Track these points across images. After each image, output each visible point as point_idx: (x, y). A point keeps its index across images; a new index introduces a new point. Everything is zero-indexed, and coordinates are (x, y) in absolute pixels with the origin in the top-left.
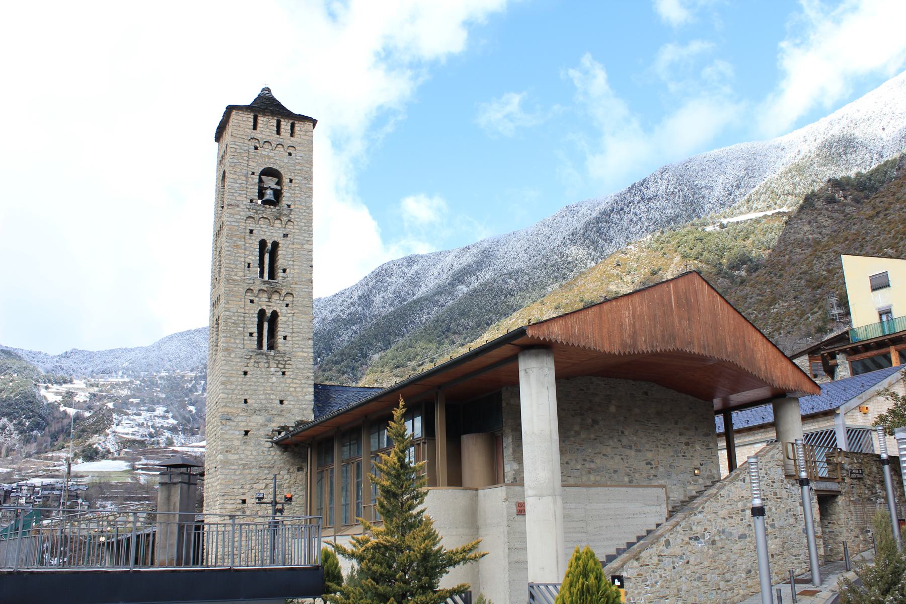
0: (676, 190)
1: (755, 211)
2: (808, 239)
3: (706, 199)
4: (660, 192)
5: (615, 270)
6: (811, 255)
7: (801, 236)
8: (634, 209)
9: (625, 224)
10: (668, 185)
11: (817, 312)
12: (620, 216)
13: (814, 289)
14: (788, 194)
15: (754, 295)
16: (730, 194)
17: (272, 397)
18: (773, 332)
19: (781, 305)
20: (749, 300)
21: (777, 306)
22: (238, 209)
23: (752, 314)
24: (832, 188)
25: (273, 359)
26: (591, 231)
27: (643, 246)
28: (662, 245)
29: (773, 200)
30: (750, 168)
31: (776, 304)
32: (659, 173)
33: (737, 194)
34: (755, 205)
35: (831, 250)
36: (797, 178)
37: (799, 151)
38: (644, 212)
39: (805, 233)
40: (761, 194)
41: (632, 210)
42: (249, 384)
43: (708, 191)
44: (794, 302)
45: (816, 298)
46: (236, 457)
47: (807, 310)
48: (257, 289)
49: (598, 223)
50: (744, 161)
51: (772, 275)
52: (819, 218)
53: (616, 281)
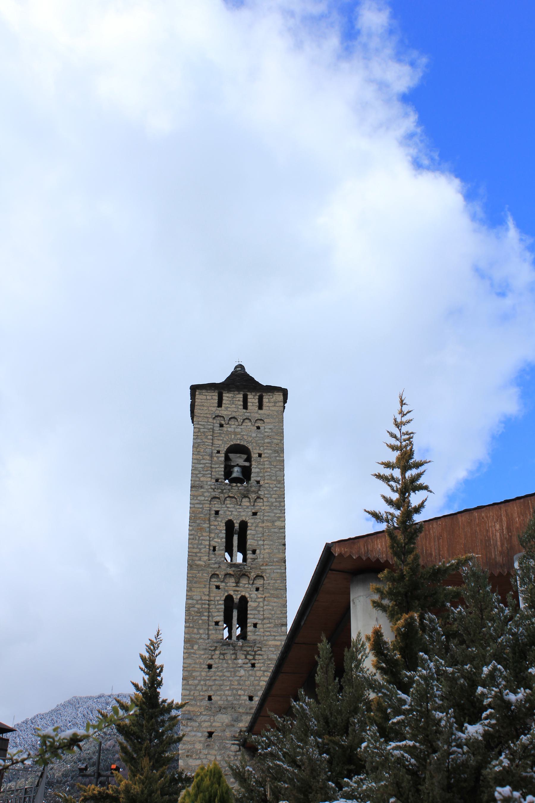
22: (202, 490)
48: (223, 573)
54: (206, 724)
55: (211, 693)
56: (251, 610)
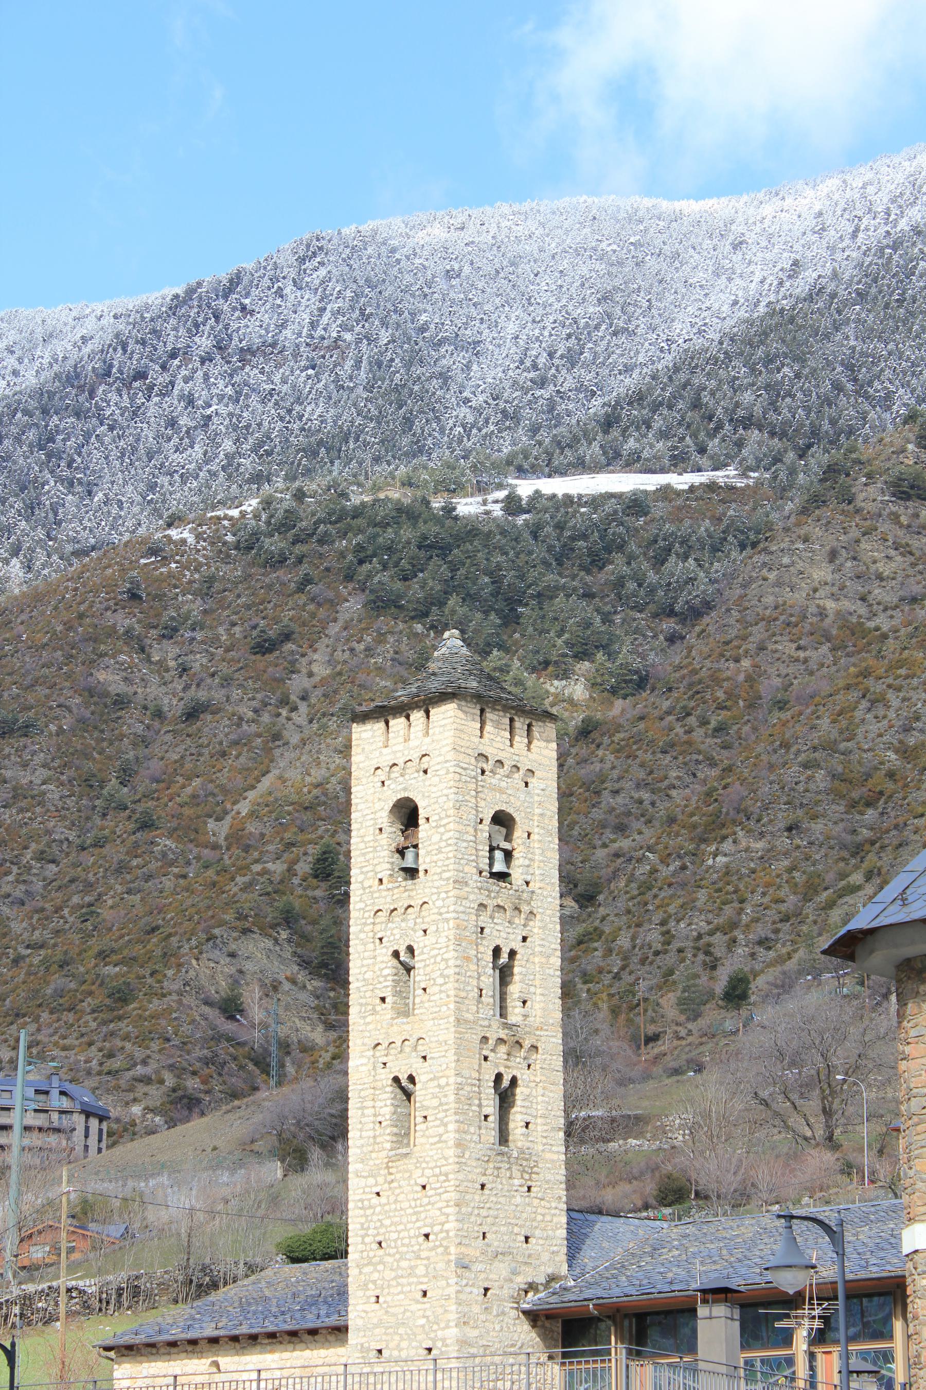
0: (348, 336)
1: (628, 465)
2: (822, 613)
3: (454, 387)
4: (287, 333)
5: (120, 615)
6: (848, 688)
7: (798, 597)
8: (186, 380)
9: (149, 434)
10: (322, 310)
11: (859, 888)
12: (132, 399)
13: (853, 805)
14: (747, 422)
15: (628, 785)
16: (542, 383)
17: (516, 1230)
18: (711, 933)
19: (744, 844)
20: (607, 799)
21: (727, 846)
22: (467, 889)
23: (639, 861)
24: (919, 445)
25: (517, 1164)
26: (18, 440)
27: (229, 538)
28: (299, 549)
29: (694, 436)
30: (618, 297)
31: (724, 838)
32: (292, 260)
33: (566, 385)
34: (631, 444)
35: (915, 681)
36: (786, 369)
37: (796, 263)
38: (221, 398)
39: (815, 590)
40: (656, 407)
41: (180, 385)
42: (488, 1205)
43: (462, 357)
44: (784, 842)
45: (859, 838)
46: (476, 1333)
47: (830, 877)
48: (495, 1036)
49: (45, 412)
50: (601, 267)
51: (692, 720)
52: (864, 545)
53: (123, 657)
54: (483, 1276)
55: (485, 1228)
56: (355, 1084)
